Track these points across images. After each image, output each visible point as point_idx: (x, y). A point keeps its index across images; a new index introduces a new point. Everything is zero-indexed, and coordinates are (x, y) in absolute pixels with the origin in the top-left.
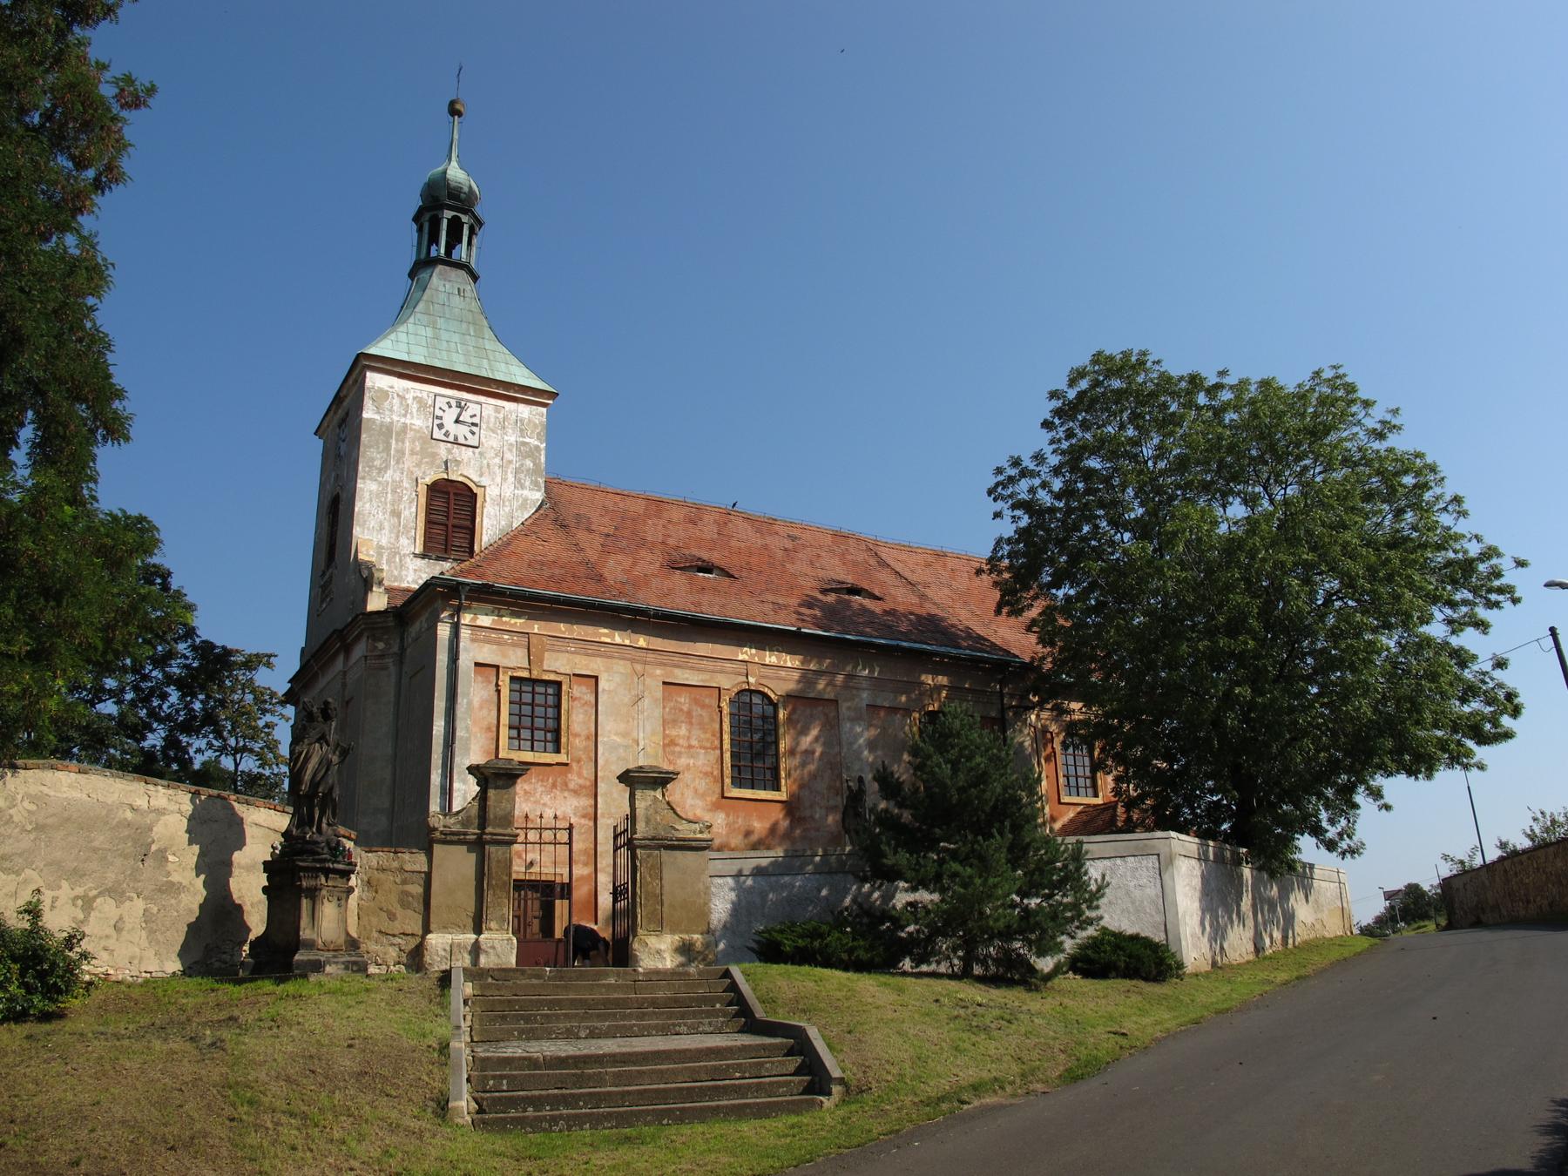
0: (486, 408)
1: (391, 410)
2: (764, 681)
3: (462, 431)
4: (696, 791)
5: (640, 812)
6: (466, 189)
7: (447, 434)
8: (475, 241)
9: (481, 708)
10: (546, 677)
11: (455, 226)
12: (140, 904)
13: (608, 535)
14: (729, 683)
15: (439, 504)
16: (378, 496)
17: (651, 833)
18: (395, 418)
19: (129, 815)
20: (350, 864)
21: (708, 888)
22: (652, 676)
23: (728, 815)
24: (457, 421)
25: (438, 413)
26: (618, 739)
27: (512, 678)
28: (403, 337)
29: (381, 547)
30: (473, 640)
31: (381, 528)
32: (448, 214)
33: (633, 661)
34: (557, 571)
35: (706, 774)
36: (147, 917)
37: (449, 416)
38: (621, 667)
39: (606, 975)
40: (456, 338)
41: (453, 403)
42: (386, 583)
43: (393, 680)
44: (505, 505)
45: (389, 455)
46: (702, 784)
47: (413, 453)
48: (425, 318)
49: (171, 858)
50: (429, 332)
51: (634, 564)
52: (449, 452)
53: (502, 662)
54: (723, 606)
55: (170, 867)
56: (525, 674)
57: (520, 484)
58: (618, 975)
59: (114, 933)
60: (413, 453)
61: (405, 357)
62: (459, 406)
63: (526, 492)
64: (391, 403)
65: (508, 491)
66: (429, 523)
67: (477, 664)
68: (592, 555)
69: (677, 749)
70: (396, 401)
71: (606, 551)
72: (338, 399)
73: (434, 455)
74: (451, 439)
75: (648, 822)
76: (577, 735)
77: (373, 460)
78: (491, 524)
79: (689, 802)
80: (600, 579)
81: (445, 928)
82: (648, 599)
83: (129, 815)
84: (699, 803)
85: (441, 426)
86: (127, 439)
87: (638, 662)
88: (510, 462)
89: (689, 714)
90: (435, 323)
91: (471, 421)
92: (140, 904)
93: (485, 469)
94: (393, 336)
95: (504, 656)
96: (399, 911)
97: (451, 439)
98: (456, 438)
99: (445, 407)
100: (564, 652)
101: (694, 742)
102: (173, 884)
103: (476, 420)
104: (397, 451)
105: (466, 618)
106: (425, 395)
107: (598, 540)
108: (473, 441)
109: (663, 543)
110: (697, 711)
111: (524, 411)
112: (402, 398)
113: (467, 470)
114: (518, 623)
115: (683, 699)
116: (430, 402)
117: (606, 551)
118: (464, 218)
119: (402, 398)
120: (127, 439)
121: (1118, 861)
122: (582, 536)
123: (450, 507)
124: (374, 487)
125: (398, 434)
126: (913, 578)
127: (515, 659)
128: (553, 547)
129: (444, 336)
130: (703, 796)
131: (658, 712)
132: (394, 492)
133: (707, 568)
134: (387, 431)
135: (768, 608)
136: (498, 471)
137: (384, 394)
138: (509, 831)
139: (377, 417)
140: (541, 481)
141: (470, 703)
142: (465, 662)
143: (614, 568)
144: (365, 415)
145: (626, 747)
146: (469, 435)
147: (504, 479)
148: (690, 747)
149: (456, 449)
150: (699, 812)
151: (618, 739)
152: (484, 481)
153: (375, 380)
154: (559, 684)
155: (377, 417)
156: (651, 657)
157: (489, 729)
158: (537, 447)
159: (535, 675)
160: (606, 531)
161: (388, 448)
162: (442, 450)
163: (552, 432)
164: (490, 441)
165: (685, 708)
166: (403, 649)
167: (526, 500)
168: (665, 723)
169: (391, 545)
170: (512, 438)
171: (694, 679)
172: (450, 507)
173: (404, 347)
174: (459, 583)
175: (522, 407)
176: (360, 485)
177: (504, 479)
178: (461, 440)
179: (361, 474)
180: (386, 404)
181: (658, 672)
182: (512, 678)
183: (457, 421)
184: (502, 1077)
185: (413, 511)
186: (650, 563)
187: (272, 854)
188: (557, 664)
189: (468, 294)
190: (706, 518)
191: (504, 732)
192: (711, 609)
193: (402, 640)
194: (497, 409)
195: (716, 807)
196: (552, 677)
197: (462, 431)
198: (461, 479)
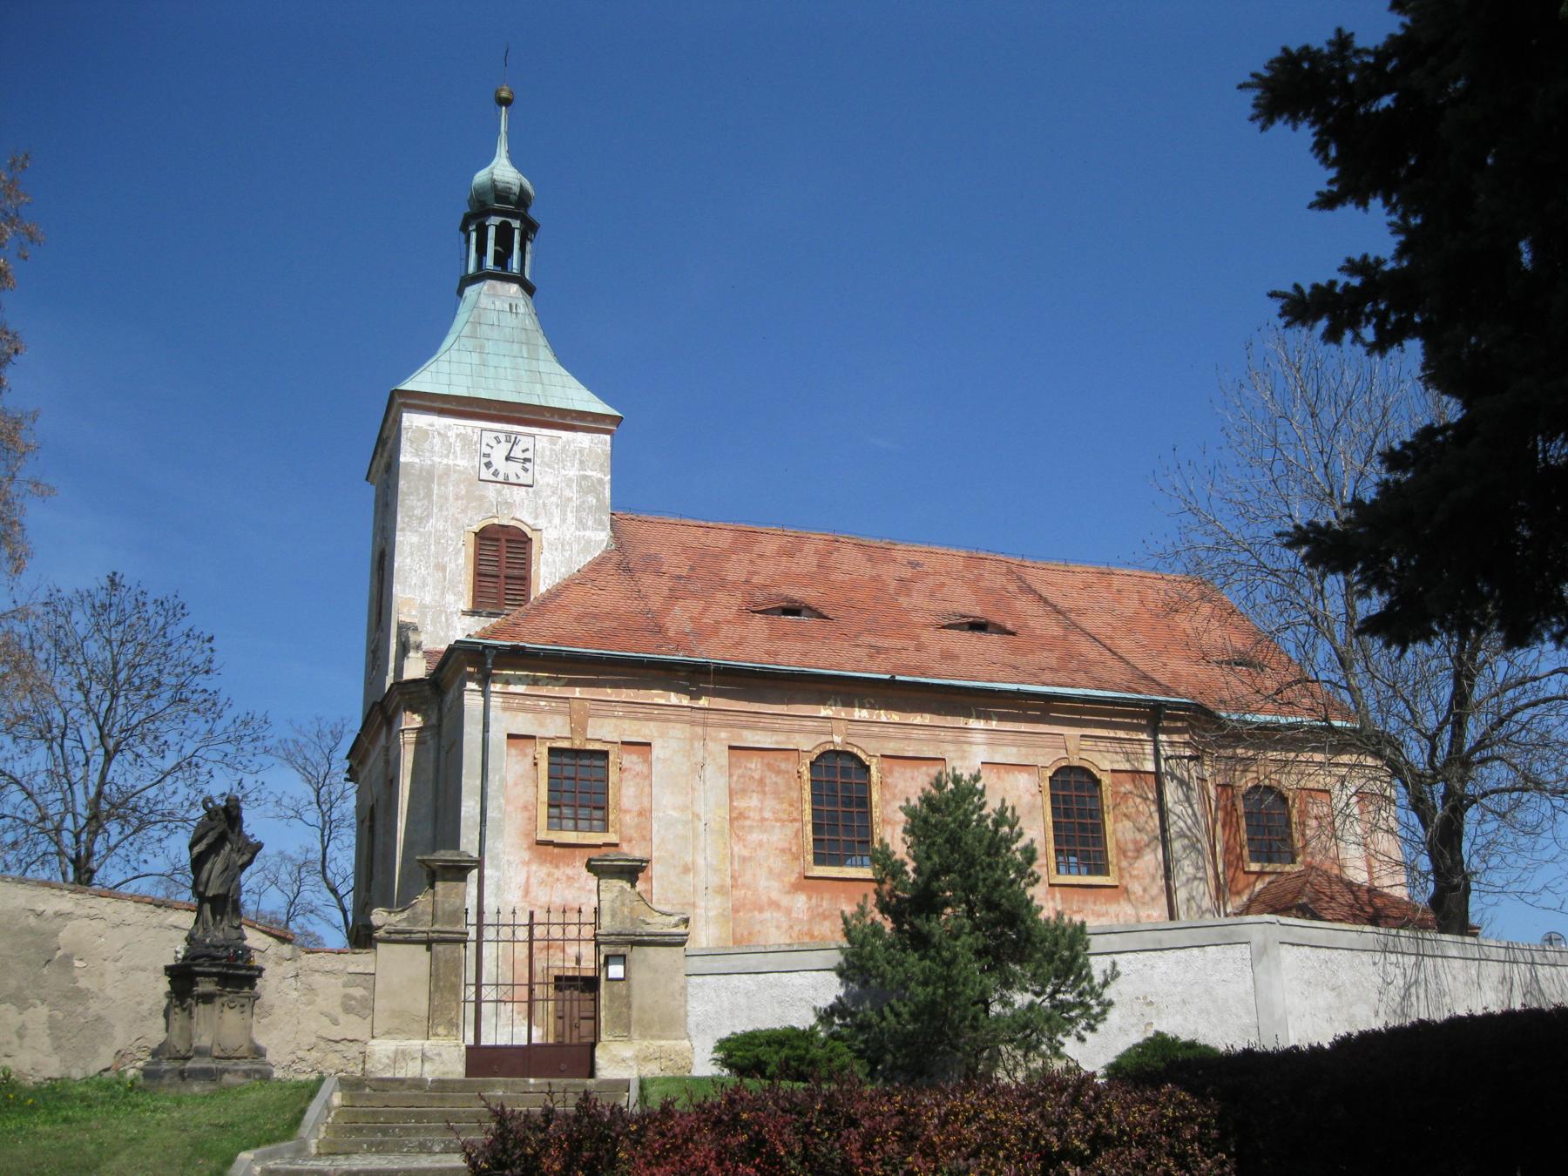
0: (542, 440)
1: (432, 451)
2: (851, 740)
3: (514, 468)
4: (770, 870)
5: (605, 905)
6: (516, 189)
7: (496, 473)
8: (529, 246)
9: (516, 784)
10: (590, 747)
11: (504, 234)
12: (43, 1011)
13: (680, 577)
14: (809, 744)
15: (489, 552)
17: (618, 928)
18: (437, 459)
19: (32, 921)
20: (252, 968)
21: (684, 988)
22: (714, 740)
23: (810, 898)
24: (508, 458)
25: (486, 450)
26: (674, 814)
27: (552, 751)
28: (444, 367)
29: (425, 606)
30: (505, 709)
31: (424, 585)
32: (495, 220)
33: (693, 723)
34: (607, 624)
35: (783, 851)
36: (53, 1025)
38: (678, 731)
39: (493, 1086)
40: (507, 362)
41: (502, 437)
42: (425, 648)
43: (432, 755)
44: (567, 544)
45: (431, 501)
46: (777, 863)
47: (457, 498)
48: (469, 343)
49: (77, 964)
50: (475, 358)
51: (705, 609)
52: (499, 493)
53: (539, 732)
54: (805, 654)
55: (77, 972)
57: (581, 525)
58: (506, 1085)
59: (15, 1039)
60: (457, 498)
61: (444, 391)
63: (588, 533)
64: (428, 442)
65: (570, 531)
66: (478, 574)
67: (510, 736)
68: (655, 602)
69: (748, 823)
70: (437, 440)
71: (673, 596)
72: (381, 441)
73: (482, 498)
74: (501, 478)
75: (613, 917)
76: (626, 811)
77: (413, 508)
78: (547, 572)
79: (763, 883)
80: (660, 629)
81: (388, 1033)
82: (711, 653)
83: (32, 921)
84: (775, 884)
85: (488, 465)
86: (1339, 31)
87: (698, 724)
88: (570, 499)
89: (761, 781)
90: (482, 347)
91: (522, 456)
92: (43, 1011)
93: (541, 511)
94: (433, 368)
95: (542, 725)
96: (342, 1018)
98: (507, 477)
99: (493, 443)
100: (607, 718)
101: (767, 815)
102: (79, 990)
103: (528, 455)
104: (440, 497)
107: (665, 584)
109: (747, 582)
110: (771, 778)
111: (582, 440)
112: (443, 436)
113: (519, 511)
115: (754, 764)
117: (673, 596)
118: (516, 224)
119: (443, 436)
120: (1339, 31)
121: (1195, 951)
122: (647, 580)
123: (502, 555)
124: (415, 539)
125: (440, 477)
126: (1063, 604)
127: (555, 728)
128: (612, 596)
129: (492, 360)
130: (780, 876)
131: (723, 781)
132: (438, 543)
133: (793, 610)
134: (428, 476)
135: (861, 653)
136: (556, 512)
137: (424, 434)
138: (458, 928)
139: (417, 460)
140: (606, 519)
141: (503, 780)
142: (497, 735)
143: (679, 618)
144: (402, 459)
145: (686, 823)
146: (521, 473)
147: (564, 520)
148: (763, 820)
150: (774, 895)
151: (674, 814)
152: (541, 523)
153: (412, 421)
154: (605, 754)
155: (417, 460)
156: (714, 717)
157: (525, 808)
158: (600, 481)
159: (577, 744)
160: (677, 572)
161: (429, 495)
162: (491, 491)
163: (619, 464)
164: (545, 477)
165: (757, 776)
166: (440, 719)
167: (588, 542)
168: (732, 794)
169: (435, 602)
170: (573, 472)
171: (766, 740)
172: (502, 555)
173: (444, 379)
174: (486, 647)
175: (580, 436)
176: (399, 537)
177: (564, 520)
178: (513, 479)
179: (399, 525)
180: (427, 446)
181: (723, 735)
182: (552, 751)
183: (508, 458)
185: (461, 563)
186: (726, 605)
187: (176, 959)
188: (603, 731)
189: (521, 310)
190: (806, 548)
191: (543, 810)
192: (789, 658)
193: (440, 710)
195: (796, 888)
196: (597, 746)
198: (512, 523)
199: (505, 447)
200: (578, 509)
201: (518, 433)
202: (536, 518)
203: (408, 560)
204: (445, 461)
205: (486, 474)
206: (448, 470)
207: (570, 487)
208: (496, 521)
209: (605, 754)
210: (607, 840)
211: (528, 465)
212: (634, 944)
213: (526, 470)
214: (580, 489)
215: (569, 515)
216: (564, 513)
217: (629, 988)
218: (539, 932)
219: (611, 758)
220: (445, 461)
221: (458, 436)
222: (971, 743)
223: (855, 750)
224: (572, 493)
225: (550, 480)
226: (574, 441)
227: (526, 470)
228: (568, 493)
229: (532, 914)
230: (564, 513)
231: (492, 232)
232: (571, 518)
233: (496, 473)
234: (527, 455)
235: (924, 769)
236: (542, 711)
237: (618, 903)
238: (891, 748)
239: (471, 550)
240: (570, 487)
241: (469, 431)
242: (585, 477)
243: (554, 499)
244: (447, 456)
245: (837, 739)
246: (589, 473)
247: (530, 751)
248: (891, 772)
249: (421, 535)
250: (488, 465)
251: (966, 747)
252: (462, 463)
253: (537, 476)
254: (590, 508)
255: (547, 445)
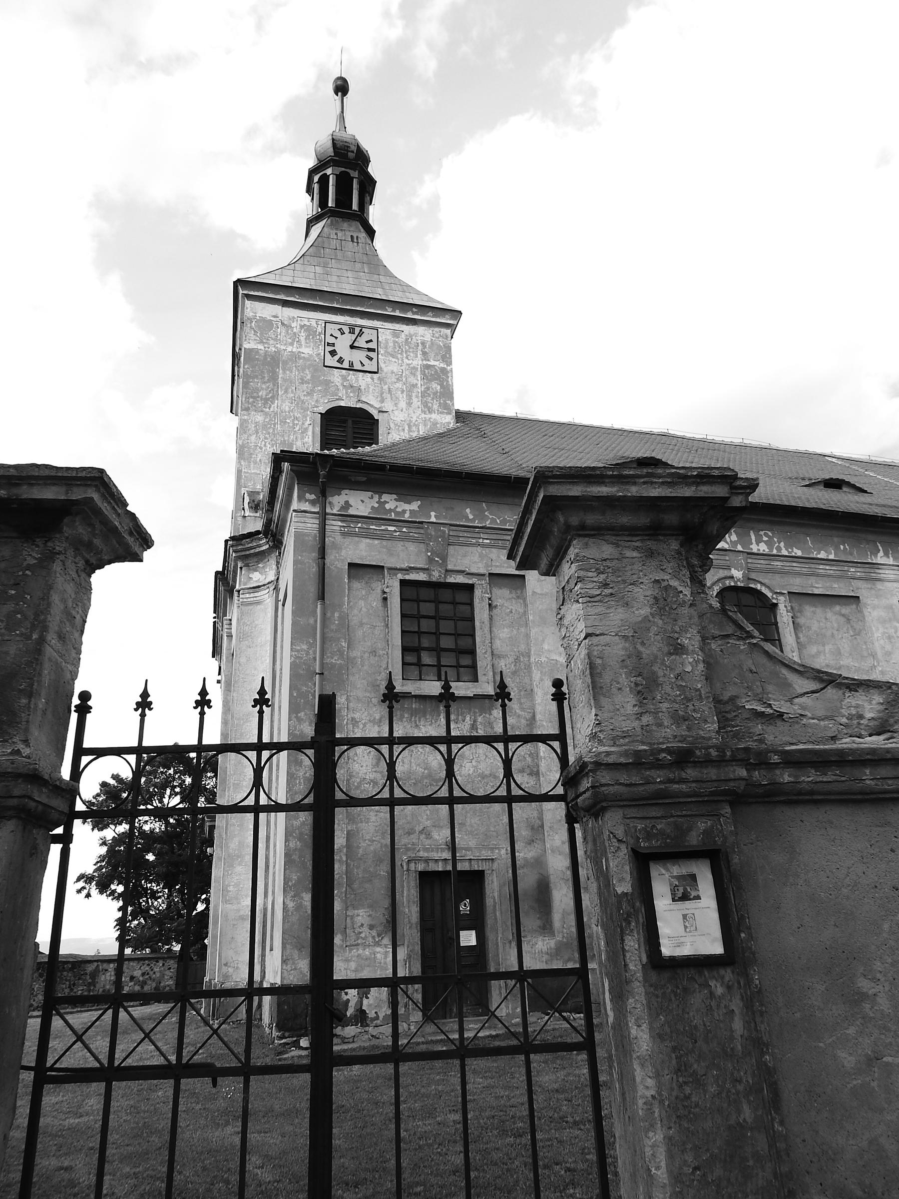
2: (753, 576)
3: (358, 357)
10: (451, 580)
16: (265, 427)
25: (331, 340)
27: (403, 583)
37: (343, 345)
40: (350, 274)
41: (346, 329)
45: (276, 384)
47: (303, 382)
52: (344, 378)
53: (389, 562)
56: (422, 577)
62: (352, 332)
77: (257, 390)
85: (333, 353)
97: (346, 365)
98: (351, 364)
99: (338, 334)
103: (372, 345)
104: (285, 380)
105: (336, 502)
106: (313, 323)
108: (370, 366)
112: (288, 327)
114: (409, 508)
116: (320, 329)
118: (354, 174)
127: (408, 557)
139: (260, 347)
146: (366, 361)
149: (352, 376)
152: (388, 406)
154: (470, 588)
155: (260, 347)
161: (274, 378)
162: (336, 377)
164: (389, 366)
170: (418, 362)
175: (421, 330)
177: (409, 404)
182: (403, 583)
184: (611, 1075)
194: (396, 333)
196: (460, 579)
197: (358, 357)
199: (348, 338)
200: (424, 394)
201: (362, 327)
202: (382, 401)
203: (253, 438)
204: (289, 349)
205: (331, 361)
206: (295, 357)
207: (414, 375)
208: (342, 404)
209: (470, 588)
210: (479, 691)
211: (371, 354)
212: (740, 799)
213: (371, 359)
214: (425, 377)
215: (415, 400)
216: (410, 397)
217: (754, 1002)
218: (360, 769)
219: (478, 593)
220: (289, 349)
221: (302, 327)
222: (880, 580)
223: (759, 587)
224: (418, 380)
225: (395, 368)
226: (416, 335)
227: (371, 359)
228: (412, 380)
229: (327, 709)
230: (410, 397)
231: (332, 181)
232: (416, 402)
233: (340, 360)
234: (370, 345)
235: (837, 608)
236: (391, 538)
237: (654, 647)
238: (798, 584)
239: (318, 429)
240: (414, 375)
241: (313, 323)
242: (428, 367)
243: (399, 385)
244: (292, 344)
245: (737, 574)
246: (432, 363)
247: (378, 587)
248: (800, 611)
249: (266, 414)
250: (333, 353)
251: (879, 585)
252: (307, 351)
253: (381, 364)
254: (435, 393)
255: (390, 337)
